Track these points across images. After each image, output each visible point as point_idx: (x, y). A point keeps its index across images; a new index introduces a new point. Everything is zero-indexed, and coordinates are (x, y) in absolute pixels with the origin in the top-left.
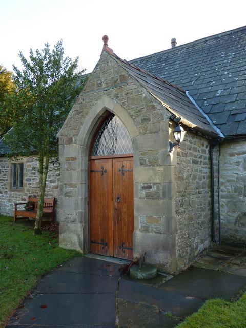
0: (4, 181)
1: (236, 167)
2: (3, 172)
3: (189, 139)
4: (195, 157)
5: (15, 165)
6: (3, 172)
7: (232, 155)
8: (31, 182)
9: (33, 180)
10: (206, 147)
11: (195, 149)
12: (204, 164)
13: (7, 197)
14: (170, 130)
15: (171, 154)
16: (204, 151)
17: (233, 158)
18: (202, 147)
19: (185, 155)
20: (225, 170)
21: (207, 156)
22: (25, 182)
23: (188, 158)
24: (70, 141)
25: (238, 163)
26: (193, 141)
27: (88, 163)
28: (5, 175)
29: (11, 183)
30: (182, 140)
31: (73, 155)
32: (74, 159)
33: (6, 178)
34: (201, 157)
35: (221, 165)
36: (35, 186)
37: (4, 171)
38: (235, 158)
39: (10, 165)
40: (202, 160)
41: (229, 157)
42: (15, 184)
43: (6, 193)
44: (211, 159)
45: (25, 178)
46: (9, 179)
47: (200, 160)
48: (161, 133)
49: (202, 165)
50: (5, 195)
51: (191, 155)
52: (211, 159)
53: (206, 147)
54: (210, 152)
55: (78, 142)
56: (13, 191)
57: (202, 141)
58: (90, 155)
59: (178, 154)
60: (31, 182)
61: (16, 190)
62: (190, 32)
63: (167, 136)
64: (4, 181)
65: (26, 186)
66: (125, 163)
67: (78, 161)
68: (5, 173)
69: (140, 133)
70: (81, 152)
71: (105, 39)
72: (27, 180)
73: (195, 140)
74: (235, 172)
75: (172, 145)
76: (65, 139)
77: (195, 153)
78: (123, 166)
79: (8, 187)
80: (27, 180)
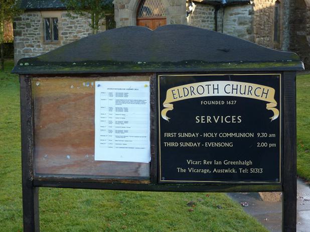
0: (35, 35)
1: (233, 23)
2: (34, 26)
3: (199, 7)
4: (204, 18)
5: (48, 19)
6: (34, 26)
7: (231, 15)
8: (68, 36)
9: (70, 33)
10: (213, 10)
11: (204, 13)
12: (210, 21)
13: (41, 50)
14: (187, 5)
15: (188, 18)
16: (210, 14)
17: (232, 17)
18: (209, 11)
19: (197, 18)
20: (227, 25)
21: (213, 16)
22: (60, 35)
23: (199, 19)
24: (123, 7)
25: (235, 21)
26: (202, 8)
27: (136, 22)
28: (36, 29)
29: (44, 37)
30: (193, 11)
31: (126, 16)
32: (127, 19)
33: (38, 32)
34: (208, 18)
35: (224, 21)
36: (72, 39)
37: (35, 25)
38: (233, 17)
39: (41, 19)
40: (209, 19)
41: (229, 16)
42: (48, 37)
43: (39, 46)
44: (216, 18)
45: (60, 32)
46: (41, 33)
47: (207, 20)
48: (182, 6)
49: (209, 23)
50: (37, 49)
51: (201, 17)
52: (216, 18)
53: (213, 10)
54: (216, 13)
55: (129, 8)
56: (47, 44)
57: (209, 7)
58: (137, 17)
59: (192, 18)
60: (68, 36)
61: (51, 43)
62: (95, 147)
63: (185, 8)
64: (35, 35)
65: (62, 38)
66: (161, 22)
67: (129, 20)
68: (35, 27)
69: (170, 5)
70: (131, 15)
71: (269, 103)
72: (62, 34)
73: (204, 7)
74: (233, 26)
75: (188, 13)
76: (119, 5)
77: (203, 16)
78: (160, 25)
79: (41, 41)
80: (62, 34)
